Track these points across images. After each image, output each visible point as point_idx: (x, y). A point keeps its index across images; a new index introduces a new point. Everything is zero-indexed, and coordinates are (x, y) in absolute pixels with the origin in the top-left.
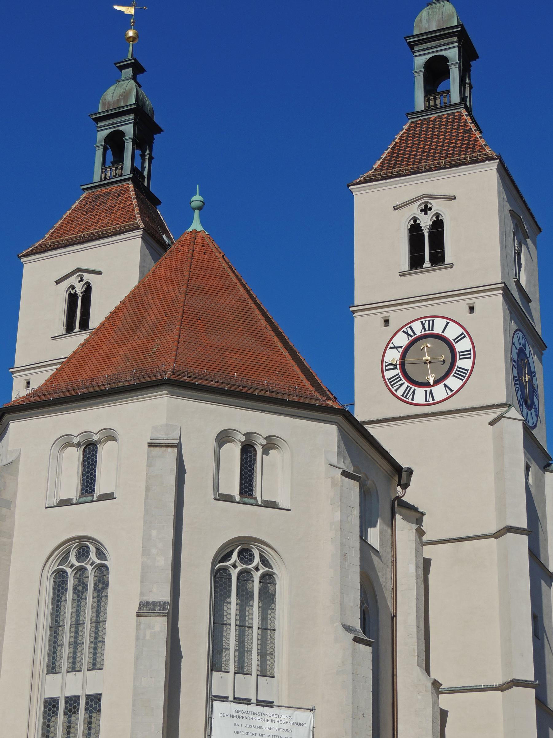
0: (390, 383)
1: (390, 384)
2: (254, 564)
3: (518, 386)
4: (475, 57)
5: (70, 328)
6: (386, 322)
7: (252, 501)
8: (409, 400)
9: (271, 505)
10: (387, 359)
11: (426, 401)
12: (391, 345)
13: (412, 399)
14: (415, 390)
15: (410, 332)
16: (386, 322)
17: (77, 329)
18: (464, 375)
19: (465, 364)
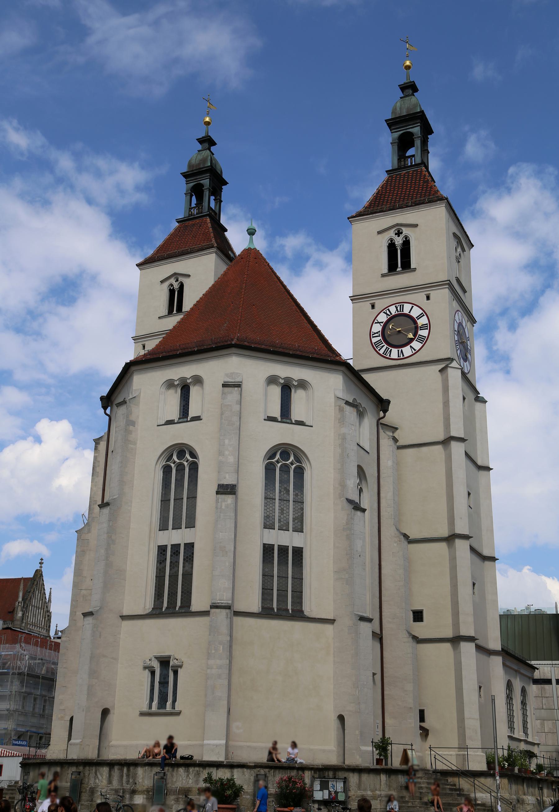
0: (375, 345)
3: (458, 347)
4: (431, 132)
5: (170, 312)
6: (373, 306)
7: (288, 421)
9: (300, 423)
11: (399, 357)
12: (376, 321)
13: (390, 356)
14: (391, 349)
15: (388, 313)
16: (373, 306)
17: (175, 312)
18: (424, 340)
19: (424, 333)
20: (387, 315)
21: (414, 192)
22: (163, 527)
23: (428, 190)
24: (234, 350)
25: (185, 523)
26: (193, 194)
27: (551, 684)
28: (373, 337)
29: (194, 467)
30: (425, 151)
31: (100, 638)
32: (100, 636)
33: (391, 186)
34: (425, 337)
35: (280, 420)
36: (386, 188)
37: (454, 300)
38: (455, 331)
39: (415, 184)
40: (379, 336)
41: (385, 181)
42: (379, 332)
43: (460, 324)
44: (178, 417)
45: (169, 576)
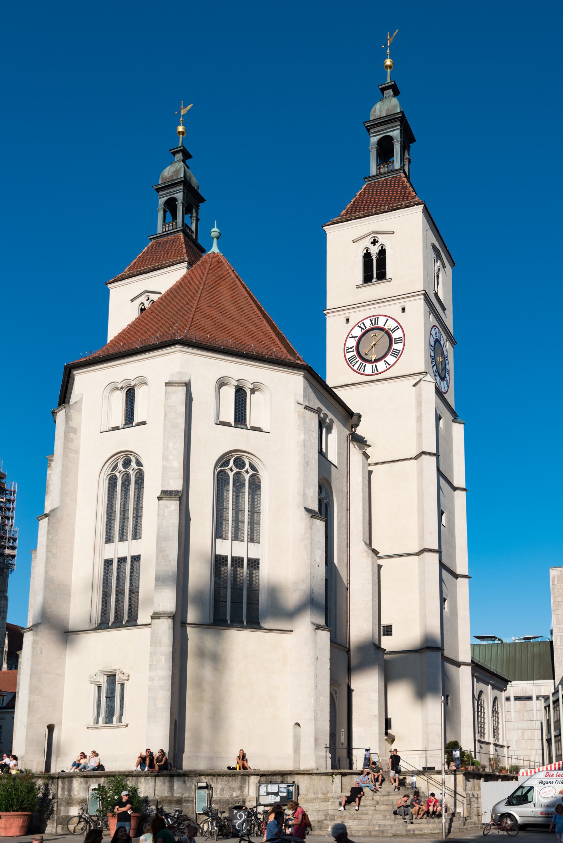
0: (349, 361)
2: (245, 469)
4: (413, 140)
8: (362, 372)
11: (373, 372)
12: (350, 336)
18: (397, 354)
20: (362, 328)
24: (178, 348)
28: (347, 352)
35: (233, 425)
38: (431, 346)
39: (393, 191)
40: (354, 351)
42: (353, 347)
43: (437, 341)
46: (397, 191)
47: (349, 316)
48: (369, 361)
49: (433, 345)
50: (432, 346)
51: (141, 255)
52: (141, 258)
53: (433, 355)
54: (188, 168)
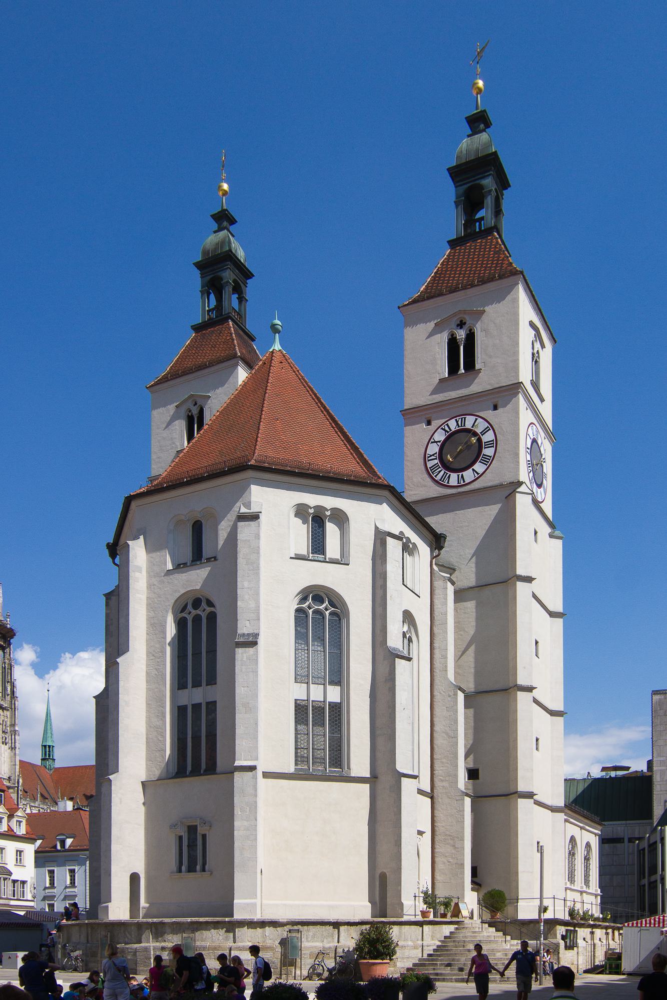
0: (431, 470)
1: (429, 472)
3: (531, 468)
10: (430, 452)
11: (458, 483)
12: (432, 440)
13: (448, 483)
14: (450, 475)
15: (447, 428)
17: (462, 371)
18: (488, 461)
19: (489, 452)
20: (446, 431)
21: (481, 267)
22: (212, 706)
23: (500, 264)
25: (205, 680)
26: (211, 291)
27: (623, 842)
28: (429, 460)
29: (212, 617)
30: (498, 212)
31: (121, 804)
32: (121, 802)
33: (453, 261)
34: (490, 457)
36: (448, 264)
37: (527, 409)
38: (528, 448)
39: (483, 257)
40: (436, 459)
41: (446, 256)
42: (436, 453)
43: (534, 441)
44: (191, 559)
45: (192, 738)
46: (488, 258)
47: (431, 417)
48: (479, 440)
49: (529, 447)
50: (529, 449)
51: (184, 350)
52: (184, 353)
53: (530, 459)
54: (233, 236)
